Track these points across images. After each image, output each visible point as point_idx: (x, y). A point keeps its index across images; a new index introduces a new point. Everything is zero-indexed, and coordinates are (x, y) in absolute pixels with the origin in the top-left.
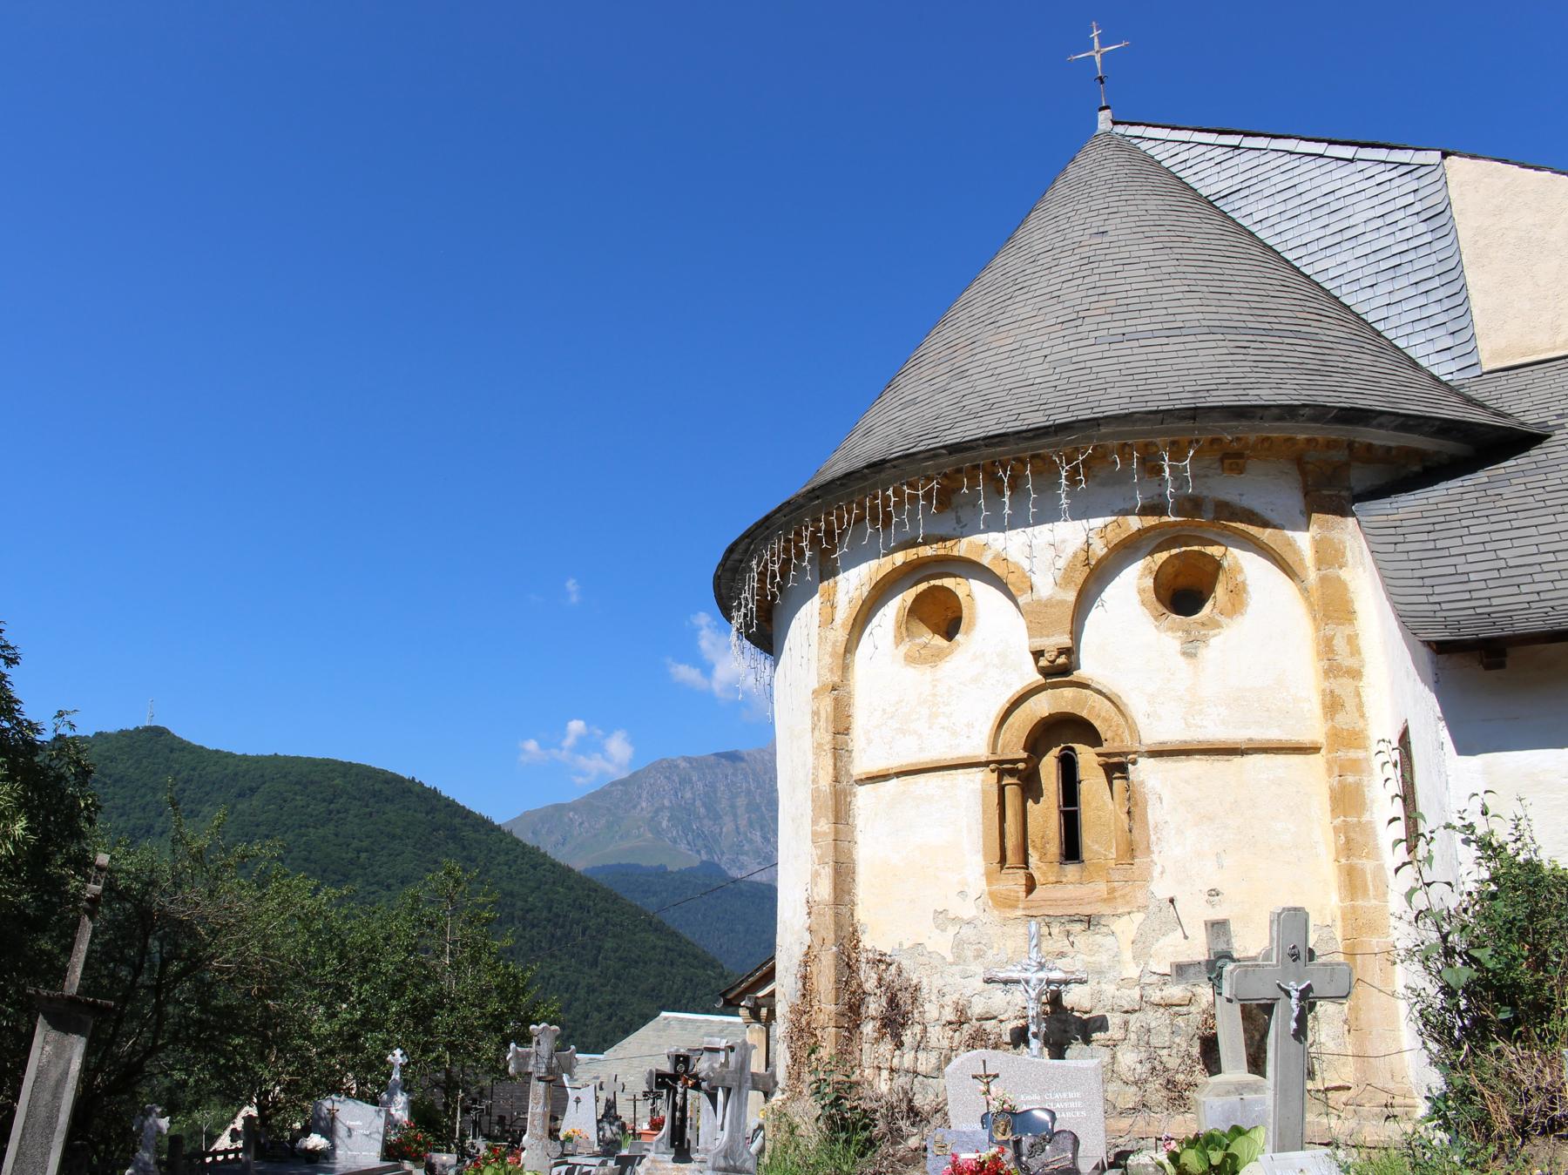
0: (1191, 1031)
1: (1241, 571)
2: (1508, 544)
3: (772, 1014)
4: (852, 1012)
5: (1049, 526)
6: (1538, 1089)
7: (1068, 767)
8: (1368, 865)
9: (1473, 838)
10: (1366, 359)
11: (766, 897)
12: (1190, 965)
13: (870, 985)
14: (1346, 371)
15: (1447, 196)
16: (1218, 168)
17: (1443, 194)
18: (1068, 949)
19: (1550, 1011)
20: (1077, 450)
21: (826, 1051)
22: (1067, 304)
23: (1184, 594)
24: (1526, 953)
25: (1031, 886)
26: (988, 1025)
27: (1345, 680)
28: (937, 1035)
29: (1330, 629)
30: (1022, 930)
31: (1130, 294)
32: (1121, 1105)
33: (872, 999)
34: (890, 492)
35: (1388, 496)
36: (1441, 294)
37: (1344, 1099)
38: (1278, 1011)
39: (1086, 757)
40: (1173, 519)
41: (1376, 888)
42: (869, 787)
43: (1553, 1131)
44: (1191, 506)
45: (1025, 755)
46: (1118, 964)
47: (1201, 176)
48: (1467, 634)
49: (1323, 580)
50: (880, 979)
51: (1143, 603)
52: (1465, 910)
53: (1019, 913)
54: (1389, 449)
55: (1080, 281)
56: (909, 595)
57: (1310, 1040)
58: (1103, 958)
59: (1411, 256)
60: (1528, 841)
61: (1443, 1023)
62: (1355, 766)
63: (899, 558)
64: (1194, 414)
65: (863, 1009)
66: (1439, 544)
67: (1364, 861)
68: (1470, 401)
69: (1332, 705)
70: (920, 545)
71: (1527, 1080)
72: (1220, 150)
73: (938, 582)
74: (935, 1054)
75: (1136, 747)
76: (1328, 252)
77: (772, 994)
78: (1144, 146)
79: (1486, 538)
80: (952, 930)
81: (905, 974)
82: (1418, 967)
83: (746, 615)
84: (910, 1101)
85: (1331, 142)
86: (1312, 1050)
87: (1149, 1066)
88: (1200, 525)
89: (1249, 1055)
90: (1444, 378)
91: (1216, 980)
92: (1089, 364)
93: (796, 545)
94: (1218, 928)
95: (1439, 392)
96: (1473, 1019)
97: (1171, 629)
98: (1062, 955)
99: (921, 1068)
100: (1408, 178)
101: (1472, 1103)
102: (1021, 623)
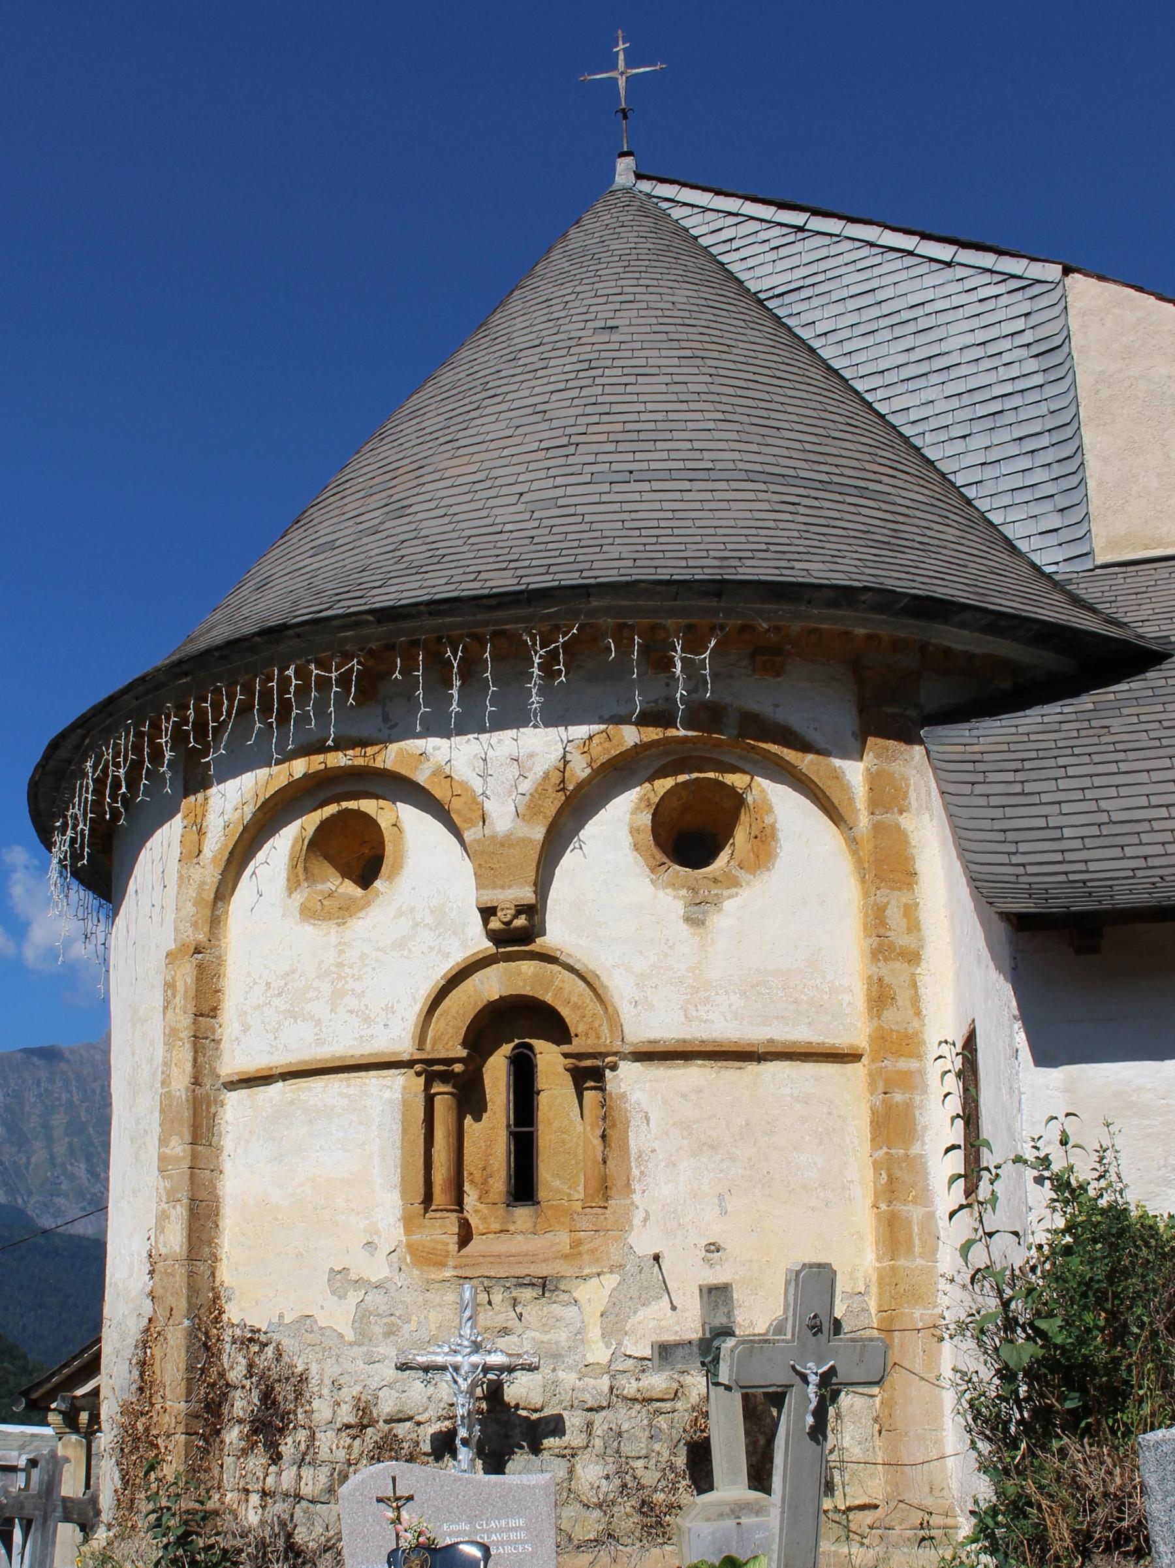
0: (676, 1435)
1: (770, 810)
2: (1113, 792)
3: (95, 1418)
4: (209, 1413)
5: (512, 733)
6: (1106, 1495)
7: (523, 1072)
8: (916, 1213)
9: (1046, 1174)
10: (951, 533)
11: (92, 1255)
12: (677, 1345)
13: (236, 1374)
14: (924, 548)
15: (1066, 326)
16: (773, 255)
17: (1060, 322)
18: (513, 1323)
19: (1126, 1397)
20: (556, 629)
21: (171, 1469)
22: (555, 424)
23: (692, 837)
24: (1102, 1323)
25: (465, 1236)
26: (401, 1429)
27: (898, 965)
28: (327, 1441)
29: (882, 895)
30: (451, 1297)
31: (643, 417)
32: (579, 1535)
33: (238, 1393)
34: (290, 672)
35: (966, 719)
36: (1050, 456)
37: (869, 1521)
38: (790, 1401)
39: (549, 1058)
40: (682, 733)
41: (923, 1243)
42: (243, 1093)
43: (1118, 1546)
44: (706, 716)
45: (463, 1053)
46: (585, 1342)
47: (751, 263)
48: (1055, 906)
49: (878, 828)
50: (251, 1366)
51: (636, 847)
52: (1033, 1269)
53: (448, 1273)
54: (972, 657)
55: (575, 393)
56: (310, 822)
57: (829, 1445)
58: (562, 1336)
59: (1016, 401)
60: (1114, 1178)
61: (998, 1415)
62: (910, 1081)
63: (300, 767)
64: (719, 589)
65: (225, 1409)
66: (1028, 788)
67: (911, 1207)
68: (1077, 601)
69: (880, 997)
70: (330, 749)
71: (1094, 1488)
72: (778, 231)
73: (352, 805)
74: (325, 1470)
75: (617, 1046)
76: (912, 385)
77: (96, 1392)
78: (676, 213)
79: (1087, 782)
80: (354, 1297)
81: (286, 1359)
82: (971, 1344)
83: (73, 841)
84: (289, 1536)
85: (925, 236)
86: (832, 1457)
87: (618, 1482)
88: (719, 744)
89: (750, 1466)
90: (1048, 569)
91: (710, 1365)
92: (580, 510)
93: (151, 742)
94: (717, 1295)
95: (1041, 586)
96: (1035, 1412)
97: (672, 885)
98: (505, 1331)
99: (306, 1490)
100: (1019, 296)
101: (1026, 1517)
102: (467, 867)
